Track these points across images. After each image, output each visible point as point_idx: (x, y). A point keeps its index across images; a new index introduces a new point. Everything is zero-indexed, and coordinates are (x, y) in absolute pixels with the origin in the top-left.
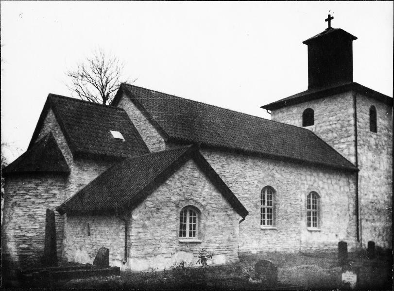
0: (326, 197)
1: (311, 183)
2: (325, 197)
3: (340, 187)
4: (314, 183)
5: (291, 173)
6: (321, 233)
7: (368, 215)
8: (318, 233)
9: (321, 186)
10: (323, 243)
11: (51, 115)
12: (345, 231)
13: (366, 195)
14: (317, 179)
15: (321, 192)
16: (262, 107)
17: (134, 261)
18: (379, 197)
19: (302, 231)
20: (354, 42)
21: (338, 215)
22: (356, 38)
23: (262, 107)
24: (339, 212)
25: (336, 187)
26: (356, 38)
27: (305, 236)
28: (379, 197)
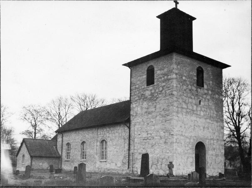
0: (110, 141)
1: (103, 135)
2: (109, 142)
3: (119, 134)
4: (104, 135)
5: (93, 133)
6: (107, 163)
7: (142, 149)
8: (105, 162)
9: (108, 136)
10: (107, 169)
11: (24, 145)
12: (121, 161)
13: (140, 135)
14: (106, 133)
15: (108, 139)
16: (125, 65)
17: (243, 99)
18: (153, 135)
19: (97, 162)
20: (193, 22)
21: (117, 151)
22: (194, 19)
23: (125, 65)
24: (118, 150)
25: (117, 134)
26: (194, 19)
27: (98, 164)
28: (153, 135)
